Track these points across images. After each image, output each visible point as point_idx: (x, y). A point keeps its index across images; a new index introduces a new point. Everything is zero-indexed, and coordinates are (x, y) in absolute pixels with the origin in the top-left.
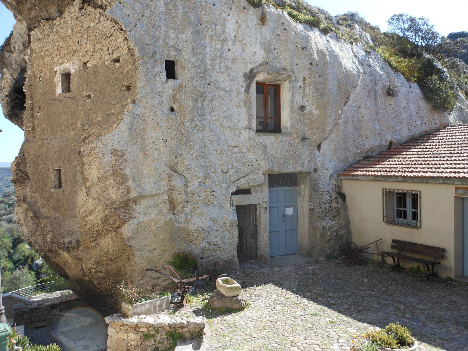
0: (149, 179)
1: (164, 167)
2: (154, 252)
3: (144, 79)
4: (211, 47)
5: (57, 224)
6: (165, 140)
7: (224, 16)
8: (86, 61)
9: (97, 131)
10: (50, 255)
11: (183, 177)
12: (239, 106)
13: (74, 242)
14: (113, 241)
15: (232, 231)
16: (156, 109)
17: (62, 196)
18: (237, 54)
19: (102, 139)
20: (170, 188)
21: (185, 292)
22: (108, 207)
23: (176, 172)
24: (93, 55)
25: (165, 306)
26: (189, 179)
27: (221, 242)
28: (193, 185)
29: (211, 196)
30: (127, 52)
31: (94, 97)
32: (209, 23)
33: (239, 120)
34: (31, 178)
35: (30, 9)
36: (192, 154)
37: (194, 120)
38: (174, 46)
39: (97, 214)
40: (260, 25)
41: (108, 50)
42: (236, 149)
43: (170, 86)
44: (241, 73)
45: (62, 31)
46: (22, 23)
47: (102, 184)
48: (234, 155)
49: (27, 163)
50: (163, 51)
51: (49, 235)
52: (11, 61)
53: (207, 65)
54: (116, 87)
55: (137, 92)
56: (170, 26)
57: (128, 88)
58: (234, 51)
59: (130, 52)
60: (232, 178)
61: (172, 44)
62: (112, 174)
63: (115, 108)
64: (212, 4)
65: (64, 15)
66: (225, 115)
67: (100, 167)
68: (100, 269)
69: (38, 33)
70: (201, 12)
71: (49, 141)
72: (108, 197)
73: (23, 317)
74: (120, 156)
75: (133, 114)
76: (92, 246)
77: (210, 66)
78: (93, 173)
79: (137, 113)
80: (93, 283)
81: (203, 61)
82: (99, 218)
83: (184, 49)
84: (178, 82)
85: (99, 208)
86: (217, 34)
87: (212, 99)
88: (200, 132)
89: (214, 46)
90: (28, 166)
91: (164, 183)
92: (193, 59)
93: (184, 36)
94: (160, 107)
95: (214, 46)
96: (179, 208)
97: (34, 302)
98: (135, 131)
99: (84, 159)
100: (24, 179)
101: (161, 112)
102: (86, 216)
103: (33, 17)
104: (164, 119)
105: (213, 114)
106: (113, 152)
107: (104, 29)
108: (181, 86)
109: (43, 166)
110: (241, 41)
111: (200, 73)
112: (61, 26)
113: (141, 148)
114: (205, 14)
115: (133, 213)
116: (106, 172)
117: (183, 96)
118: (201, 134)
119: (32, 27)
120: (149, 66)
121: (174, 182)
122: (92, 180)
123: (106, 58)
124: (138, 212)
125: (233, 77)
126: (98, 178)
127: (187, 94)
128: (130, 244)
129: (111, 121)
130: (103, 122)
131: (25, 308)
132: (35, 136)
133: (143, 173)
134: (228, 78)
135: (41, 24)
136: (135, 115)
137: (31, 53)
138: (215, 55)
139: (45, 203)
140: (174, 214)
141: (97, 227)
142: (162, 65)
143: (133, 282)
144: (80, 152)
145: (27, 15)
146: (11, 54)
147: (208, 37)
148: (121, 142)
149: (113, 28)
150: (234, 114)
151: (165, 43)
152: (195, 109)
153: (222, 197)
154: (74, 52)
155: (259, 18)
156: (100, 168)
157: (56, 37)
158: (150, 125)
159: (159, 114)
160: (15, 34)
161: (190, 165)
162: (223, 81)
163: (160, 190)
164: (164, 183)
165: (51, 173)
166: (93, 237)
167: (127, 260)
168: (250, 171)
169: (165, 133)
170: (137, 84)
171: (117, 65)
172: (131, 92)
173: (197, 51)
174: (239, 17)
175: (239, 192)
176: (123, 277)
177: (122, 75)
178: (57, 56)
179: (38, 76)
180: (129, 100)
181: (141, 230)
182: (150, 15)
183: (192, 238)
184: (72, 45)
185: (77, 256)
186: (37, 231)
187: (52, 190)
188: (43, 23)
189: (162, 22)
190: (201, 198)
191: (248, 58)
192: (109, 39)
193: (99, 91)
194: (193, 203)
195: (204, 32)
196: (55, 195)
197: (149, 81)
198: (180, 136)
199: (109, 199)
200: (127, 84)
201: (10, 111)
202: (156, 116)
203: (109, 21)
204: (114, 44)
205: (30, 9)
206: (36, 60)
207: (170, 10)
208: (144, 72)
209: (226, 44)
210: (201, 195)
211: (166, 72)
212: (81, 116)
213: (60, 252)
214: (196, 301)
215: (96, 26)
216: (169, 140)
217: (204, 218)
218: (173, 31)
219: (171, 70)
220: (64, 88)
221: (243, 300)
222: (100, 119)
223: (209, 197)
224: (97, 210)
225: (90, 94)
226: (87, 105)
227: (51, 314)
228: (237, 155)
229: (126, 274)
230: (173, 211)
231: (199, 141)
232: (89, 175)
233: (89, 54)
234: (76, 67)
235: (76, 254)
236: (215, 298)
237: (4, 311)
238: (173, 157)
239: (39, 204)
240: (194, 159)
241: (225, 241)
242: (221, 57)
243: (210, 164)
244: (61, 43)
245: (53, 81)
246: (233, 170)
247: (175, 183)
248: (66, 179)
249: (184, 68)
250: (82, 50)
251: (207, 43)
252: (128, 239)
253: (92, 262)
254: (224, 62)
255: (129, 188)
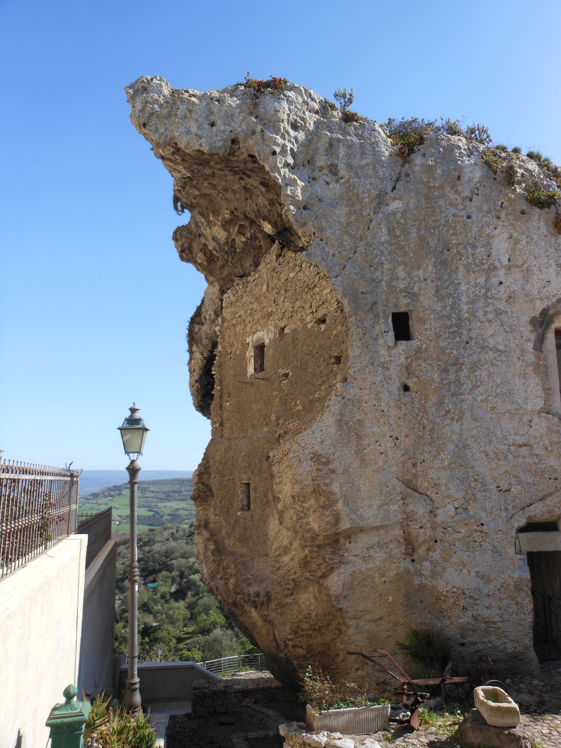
0: (369, 500)
1: (395, 481)
2: (378, 623)
3: (360, 345)
4: (467, 285)
5: (243, 565)
6: (394, 437)
7: (488, 231)
8: (283, 325)
9: (295, 426)
10: (235, 610)
11: (428, 499)
12: (526, 374)
13: (262, 593)
14: (316, 599)
15: (520, 600)
16: (379, 389)
17: (250, 522)
18: (514, 288)
19: (298, 438)
20: (405, 516)
21: (417, 703)
22: (308, 544)
23: (415, 490)
24: (292, 316)
25: (380, 723)
26: (438, 501)
27: (500, 619)
28: (446, 513)
29: (479, 533)
30: (336, 307)
31: (292, 376)
32: (461, 247)
33: (526, 399)
34: (215, 494)
35: (223, 267)
36: (442, 460)
37: (443, 403)
38: (405, 290)
39: (294, 553)
40: (553, 234)
41: (311, 307)
42: (523, 449)
43: (401, 352)
44: (526, 319)
45: (257, 289)
46: (214, 285)
47: (298, 507)
48: (519, 460)
49: (212, 472)
50: (387, 300)
51: (232, 581)
52: (201, 336)
53: (463, 312)
54: (322, 359)
55: (348, 364)
56: (398, 261)
57: (338, 360)
58: (508, 284)
59: (339, 307)
60: (517, 501)
61: (402, 286)
62: (312, 492)
63: (320, 390)
64: (465, 217)
65: (259, 268)
66: (499, 391)
67: (294, 481)
68: (299, 642)
69: (231, 296)
70: (447, 231)
71: (237, 441)
72: (308, 527)
73: (204, 702)
74: (324, 464)
75: (343, 398)
76: (287, 604)
77: (468, 312)
78: (286, 489)
79: (349, 397)
80: (292, 664)
81: (455, 307)
82: (296, 560)
83: (422, 292)
84: (414, 343)
85: (296, 544)
86: (477, 261)
87: (474, 367)
88: (455, 422)
89: (472, 280)
90: (212, 477)
91: (394, 507)
92: (438, 306)
93: (421, 273)
94: (386, 386)
95: (472, 280)
96: (421, 551)
97: (220, 681)
98: (347, 424)
99: (273, 468)
100: (207, 496)
101: (386, 394)
102: (280, 555)
103: (226, 276)
104: (392, 403)
105: (477, 392)
106: (314, 458)
107: (306, 279)
108: (419, 350)
109: (228, 477)
110: (520, 267)
111: (451, 327)
112: (255, 282)
113: (356, 451)
114: (455, 234)
115: (346, 554)
116: (303, 488)
117: (423, 365)
118: (456, 426)
119: (224, 289)
120: (366, 324)
121: (411, 507)
122: (284, 500)
123: (309, 318)
124: (353, 553)
125: (510, 327)
126: (293, 497)
127: (431, 362)
128: (341, 606)
129: (315, 411)
130: (304, 412)
131: (207, 688)
132: (223, 435)
133: (360, 491)
134: (502, 329)
135: (235, 284)
136: (346, 400)
137: (223, 322)
138: (476, 296)
139: (230, 531)
140: (413, 561)
141: (295, 573)
142: (387, 320)
143: (349, 671)
144: (269, 457)
145: (219, 275)
146: (201, 326)
147: (461, 268)
148: (325, 442)
149: (317, 276)
150: (516, 388)
151: (389, 285)
152: (444, 385)
153: (498, 536)
154: (270, 314)
155: (550, 223)
156: (295, 482)
157: (250, 297)
158: (369, 415)
159: (385, 396)
160: (206, 301)
161: (439, 478)
162: (493, 336)
163: (389, 519)
164: (394, 507)
165: (238, 487)
166: (288, 589)
167: (337, 632)
168: (552, 489)
169: (395, 426)
170: (350, 353)
171: (323, 326)
172: (341, 365)
173: (444, 292)
174: (515, 228)
175: (532, 527)
176: (334, 660)
177: (329, 341)
178: (250, 322)
179: (229, 351)
180: (339, 378)
181: (358, 585)
182: (365, 249)
183: (445, 606)
184: (267, 307)
185: (266, 616)
186: (218, 573)
187: (239, 513)
188: (237, 281)
189: (385, 257)
190: (460, 536)
191: (535, 292)
192: (312, 292)
193: (299, 368)
194: (447, 544)
195: (455, 261)
196: (241, 520)
197: (367, 347)
198: (419, 431)
199: (309, 530)
200: (335, 354)
201: (201, 401)
202: (379, 399)
203: (312, 267)
204: (318, 298)
205: (223, 267)
206: (228, 331)
207: (397, 237)
208: (358, 333)
209: (495, 275)
210: (461, 530)
211: (395, 330)
212: (276, 404)
213: (247, 607)
214: (440, 723)
215: (296, 276)
216: (402, 438)
217: (465, 571)
218: (403, 267)
219: (402, 326)
220: (257, 366)
221: (524, 738)
222: (300, 407)
223: (475, 535)
224: (293, 547)
225: (287, 372)
226: (284, 389)
227: (242, 704)
228: (526, 460)
229: (337, 655)
230: (412, 555)
231: (454, 437)
232: (280, 492)
233: (287, 316)
234: (271, 336)
235: (265, 613)
236: (469, 725)
237: (138, 686)
238: (409, 464)
239: (224, 533)
240: (445, 468)
241: (506, 616)
242: (487, 297)
243: (476, 477)
244: (255, 305)
245: (244, 357)
246: (519, 487)
247: (412, 508)
248: (256, 497)
249: (423, 321)
250: (279, 311)
251: (460, 277)
252: (336, 597)
253: (287, 630)
254: (493, 304)
255: (338, 514)
